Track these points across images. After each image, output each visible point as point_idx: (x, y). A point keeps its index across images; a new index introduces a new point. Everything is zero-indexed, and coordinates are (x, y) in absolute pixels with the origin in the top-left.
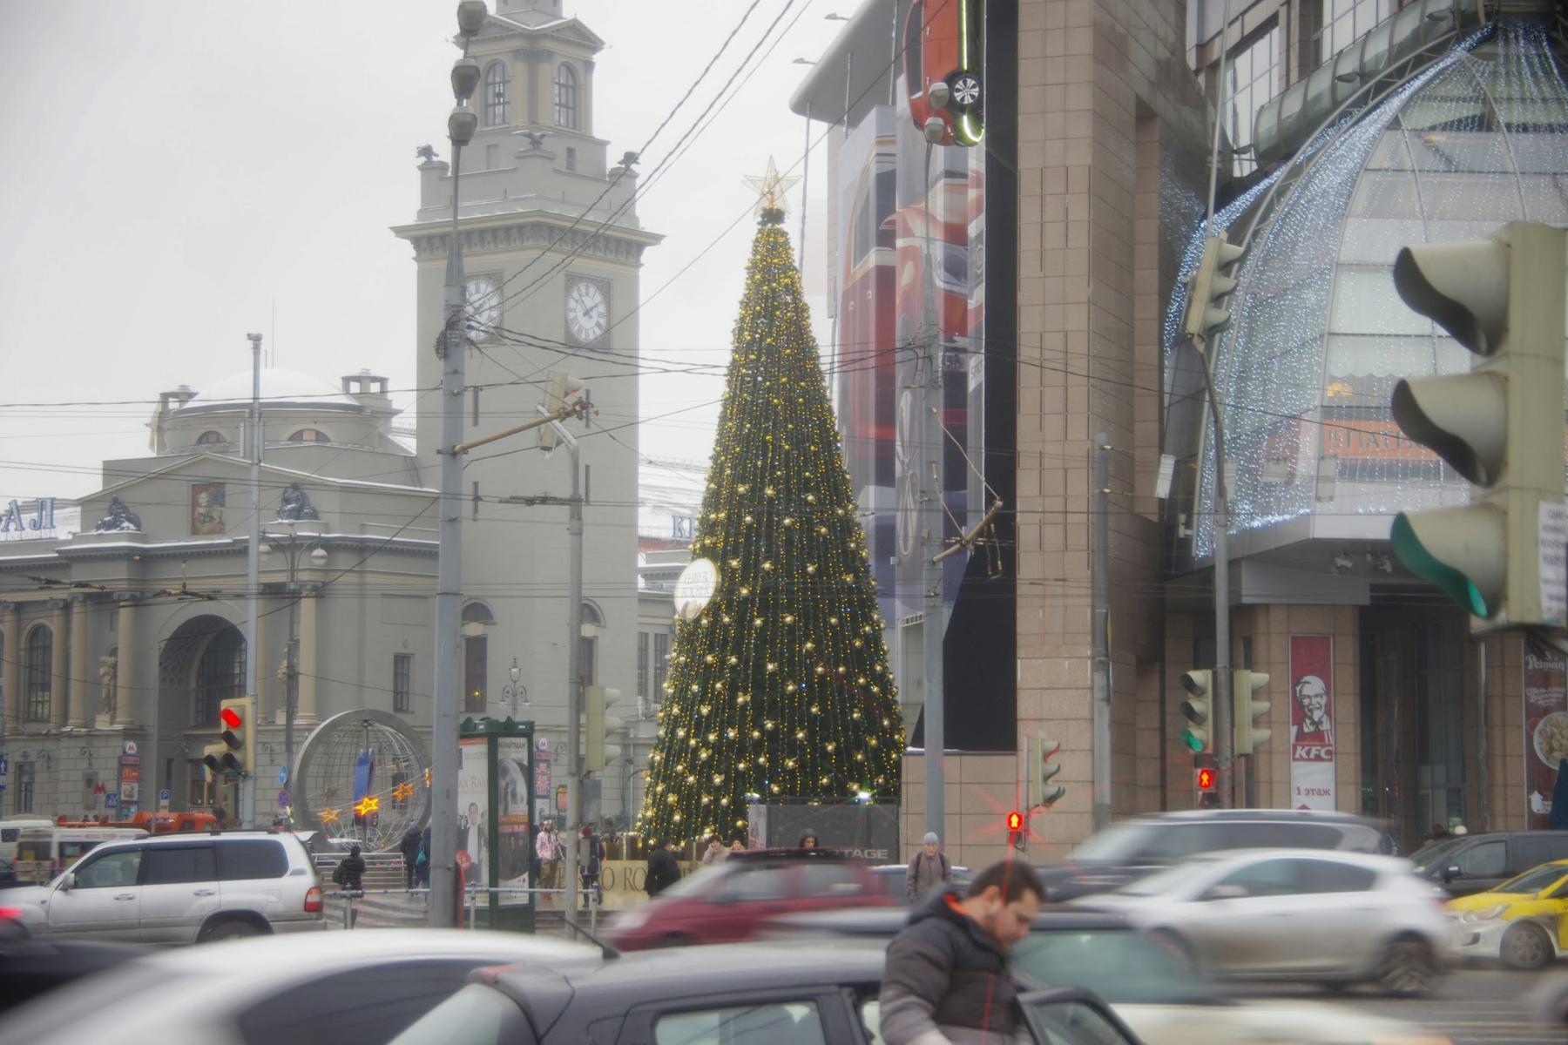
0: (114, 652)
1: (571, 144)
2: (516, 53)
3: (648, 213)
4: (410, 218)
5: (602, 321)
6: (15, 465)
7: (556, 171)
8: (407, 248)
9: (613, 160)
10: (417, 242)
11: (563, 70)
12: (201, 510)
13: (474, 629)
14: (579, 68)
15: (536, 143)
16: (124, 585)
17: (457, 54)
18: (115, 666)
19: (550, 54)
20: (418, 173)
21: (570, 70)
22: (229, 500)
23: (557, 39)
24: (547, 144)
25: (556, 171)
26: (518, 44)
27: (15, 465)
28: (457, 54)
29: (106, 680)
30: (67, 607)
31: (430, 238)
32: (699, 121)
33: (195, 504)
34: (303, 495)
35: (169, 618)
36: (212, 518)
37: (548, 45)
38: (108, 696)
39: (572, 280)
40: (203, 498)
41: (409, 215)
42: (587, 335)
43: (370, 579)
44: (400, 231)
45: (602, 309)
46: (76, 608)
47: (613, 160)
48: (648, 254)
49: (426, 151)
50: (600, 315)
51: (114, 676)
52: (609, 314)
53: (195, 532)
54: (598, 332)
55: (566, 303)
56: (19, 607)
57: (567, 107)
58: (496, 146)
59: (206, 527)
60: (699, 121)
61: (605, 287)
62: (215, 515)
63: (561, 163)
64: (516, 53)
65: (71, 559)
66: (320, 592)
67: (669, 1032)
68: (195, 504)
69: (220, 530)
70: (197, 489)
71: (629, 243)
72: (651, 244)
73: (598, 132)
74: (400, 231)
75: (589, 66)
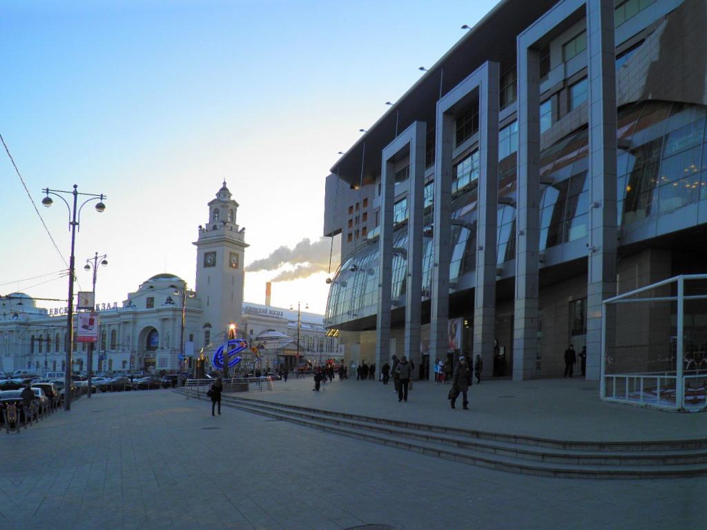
8: (196, 247)
9: (240, 229)
13: (207, 329)
14: (234, 211)
26: (222, 204)
35: (214, 224)
47: (240, 229)
49: (200, 227)
74: (194, 243)
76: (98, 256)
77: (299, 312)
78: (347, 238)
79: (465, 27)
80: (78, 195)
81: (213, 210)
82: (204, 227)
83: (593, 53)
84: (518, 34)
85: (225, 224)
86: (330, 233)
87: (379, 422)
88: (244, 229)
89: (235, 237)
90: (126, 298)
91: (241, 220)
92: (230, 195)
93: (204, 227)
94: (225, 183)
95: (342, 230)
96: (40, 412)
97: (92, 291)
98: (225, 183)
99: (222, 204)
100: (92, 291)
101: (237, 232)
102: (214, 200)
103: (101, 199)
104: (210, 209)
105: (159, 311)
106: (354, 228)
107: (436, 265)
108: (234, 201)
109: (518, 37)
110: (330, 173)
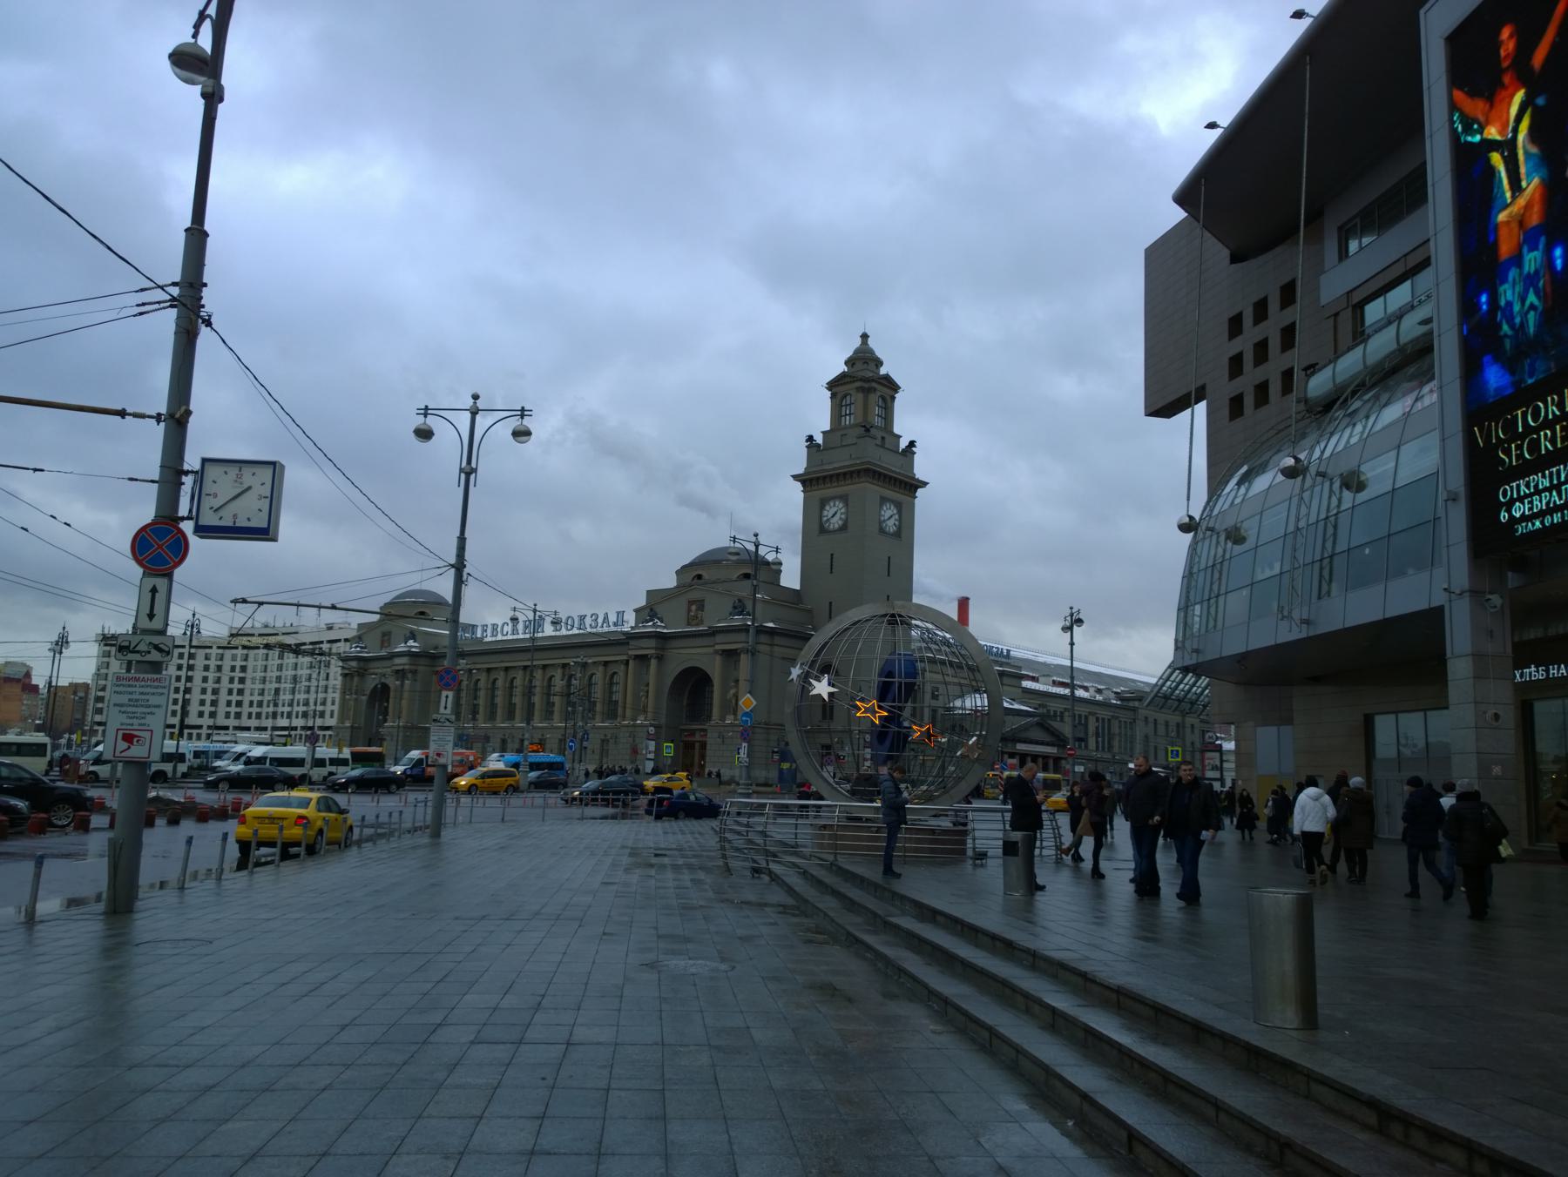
0: (648, 685)
1: (884, 435)
2: (858, 389)
3: (921, 470)
4: (801, 470)
5: (897, 523)
6: (26, 582)
7: (877, 445)
8: (799, 486)
10: (804, 483)
11: (880, 400)
12: (692, 614)
14: (888, 398)
15: (868, 430)
16: (653, 651)
17: (896, 395)
18: (647, 692)
19: (875, 390)
20: (806, 449)
21: (884, 399)
22: (706, 608)
23: (880, 383)
24: (873, 431)
25: (877, 445)
26: (858, 384)
27: (26, 582)
28: (896, 395)
29: (643, 699)
30: (627, 663)
31: (811, 480)
32: (151, 311)
33: (689, 610)
34: (743, 604)
35: (674, 668)
36: (697, 618)
37: (874, 385)
38: (644, 707)
39: (883, 500)
40: (694, 607)
41: (800, 468)
42: (829, 525)
43: (776, 649)
44: (795, 477)
45: (897, 517)
46: (631, 662)
47: (903, 444)
48: (920, 492)
49: (810, 438)
50: (896, 520)
51: (647, 697)
52: (900, 520)
53: (689, 624)
54: (840, 522)
55: (880, 512)
56: (606, 664)
57: (881, 416)
58: (845, 435)
59: (695, 622)
60: (151, 311)
61: (899, 506)
62: (699, 616)
63: (879, 442)
64: (858, 389)
65: (630, 637)
66: (753, 653)
67: (1547, 745)
68: (689, 610)
69: (701, 623)
70: (691, 603)
71: (912, 485)
72: (922, 487)
73: (896, 430)
74: (795, 477)
75: (893, 398)
76: (480, 404)
77: (1473, 655)
78: (1226, 412)
79: (1299, 15)
80: (760, 547)
81: (839, 396)
82: (819, 439)
83: (1435, 129)
84: (1421, 7)
85: (868, 430)
86: (1163, 405)
87: (1396, 1129)
88: (912, 444)
89: (890, 463)
90: (642, 602)
91: (906, 423)
92: (879, 363)
93: (819, 439)
94: (865, 337)
95: (1208, 390)
96: (693, 686)
97: (266, 526)
98: (865, 337)
99: (858, 384)
100: (266, 526)
101: (897, 452)
102: (842, 376)
103: (777, 552)
104: (833, 396)
105: (713, 632)
106: (1252, 375)
107: (1453, 498)
108: (887, 378)
109: (1422, 12)
110: (1179, 214)
